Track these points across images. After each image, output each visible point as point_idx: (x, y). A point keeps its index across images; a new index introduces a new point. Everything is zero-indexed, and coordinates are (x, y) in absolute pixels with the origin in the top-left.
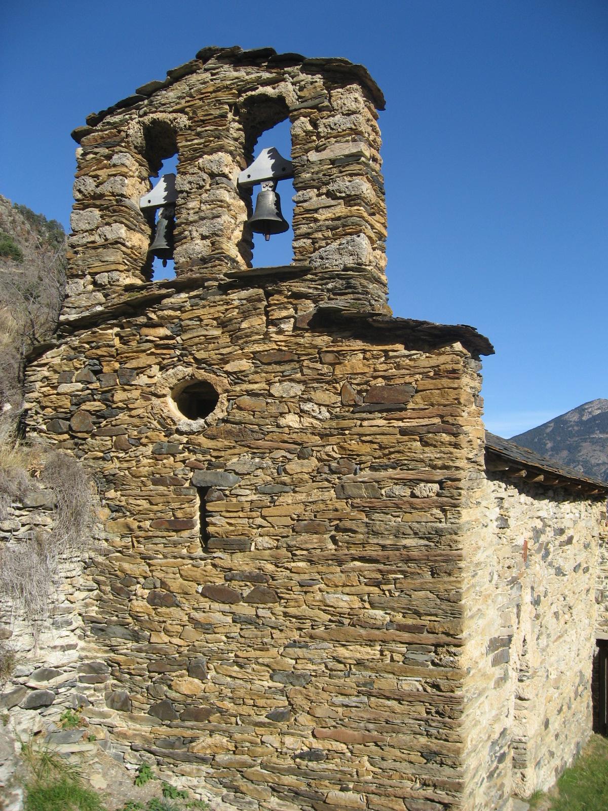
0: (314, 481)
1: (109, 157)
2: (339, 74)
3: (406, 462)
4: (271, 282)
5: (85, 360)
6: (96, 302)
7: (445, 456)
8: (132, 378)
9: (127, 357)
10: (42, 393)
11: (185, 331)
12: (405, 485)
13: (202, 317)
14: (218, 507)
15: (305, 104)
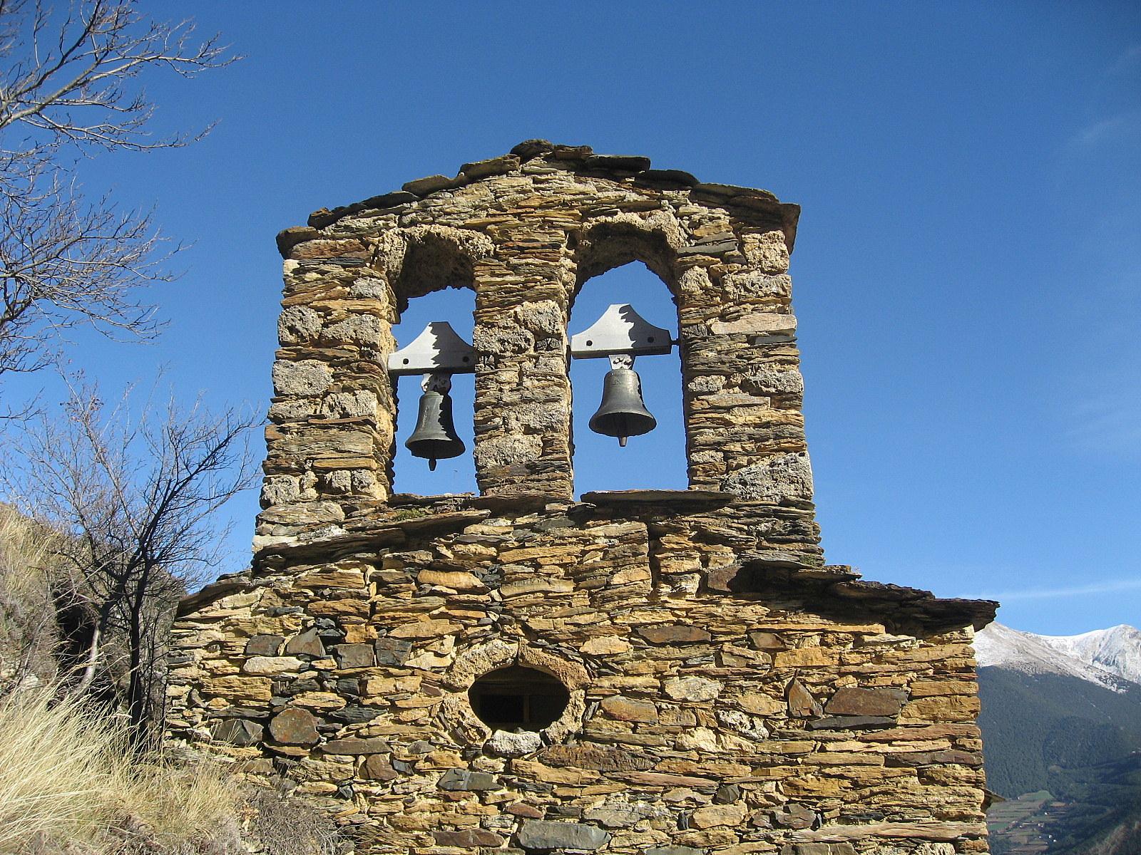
0: (742, 840)
1: (348, 282)
2: (758, 212)
3: (897, 809)
4: (662, 514)
5: (306, 617)
7: (961, 799)
8: (405, 655)
9: (393, 618)
10: (211, 670)
11: (510, 582)
12: (898, 846)
13: (541, 561)
15: (703, 248)
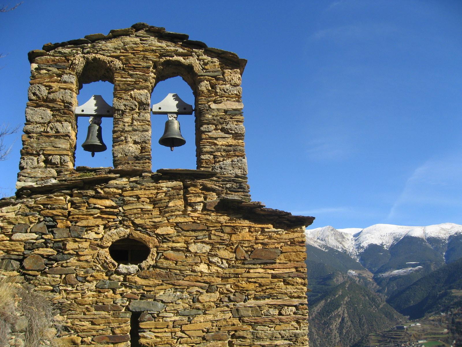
1: (60, 76)
3: (275, 294)
4: (189, 179)
6: (51, 176)
7: (299, 291)
8: (83, 233)
9: (78, 218)
13: (140, 196)
14: (149, 325)
15: (208, 74)
